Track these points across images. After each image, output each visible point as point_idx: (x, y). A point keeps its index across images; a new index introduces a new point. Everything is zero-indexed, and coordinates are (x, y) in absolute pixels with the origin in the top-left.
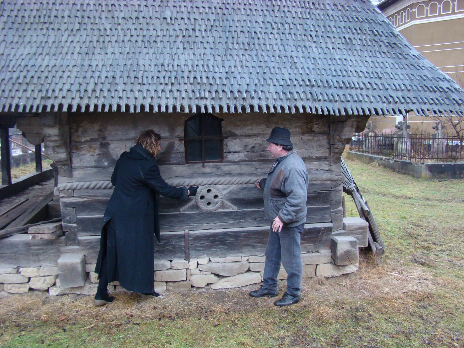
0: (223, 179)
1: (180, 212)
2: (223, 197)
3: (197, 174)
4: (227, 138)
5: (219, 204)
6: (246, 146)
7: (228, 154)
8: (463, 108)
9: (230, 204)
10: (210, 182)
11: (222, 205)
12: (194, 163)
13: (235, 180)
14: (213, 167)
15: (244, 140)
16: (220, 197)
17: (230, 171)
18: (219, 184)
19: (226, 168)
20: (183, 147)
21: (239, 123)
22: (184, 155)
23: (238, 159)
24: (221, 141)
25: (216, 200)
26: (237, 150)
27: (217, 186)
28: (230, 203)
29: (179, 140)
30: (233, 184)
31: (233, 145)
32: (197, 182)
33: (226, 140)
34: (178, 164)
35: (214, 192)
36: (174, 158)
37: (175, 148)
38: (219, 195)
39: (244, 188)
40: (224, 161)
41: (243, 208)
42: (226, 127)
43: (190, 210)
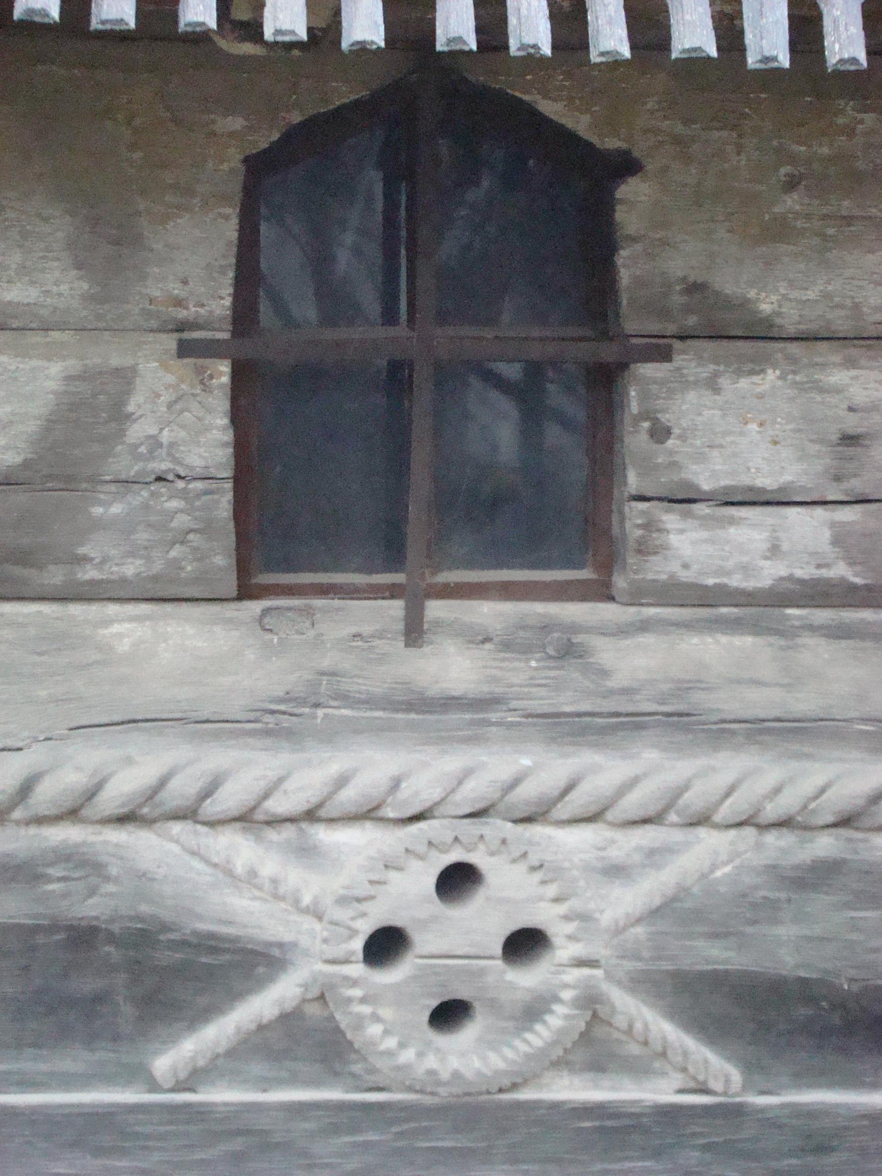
0: (603, 770)
1: (154, 1086)
2: (599, 950)
3: (345, 699)
4: (664, 355)
5: (558, 1019)
6: (850, 440)
7: (671, 519)
8: (881, 847)
9: (665, 1029)
10: (474, 791)
11: (586, 1037)
12: (325, 591)
13: (723, 780)
14: (510, 645)
15: (838, 377)
16: (564, 949)
17: (683, 688)
18: (562, 811)
19: (638, 656)
20: (223, 421)
21: (792, 202)
22: (224, 504)
23: (769, 574)
24: (604, 382)
25: (526, 979)
26: (767, 481)
27: (538, 831)
28: (673, 1014)
29: (185, 350)
30: (701, 820)
31: (720, 429)
32: (342, 781)
33: (648, 370)
34: (159, 593)
35: (509, 894)
36: (114, 533)
37: (136, 432)
38: (558, 931)
39: (819, 875)
40: (620, 582)
41: (805, 1077)
42: (661, 242)
43: (257, 1068)
